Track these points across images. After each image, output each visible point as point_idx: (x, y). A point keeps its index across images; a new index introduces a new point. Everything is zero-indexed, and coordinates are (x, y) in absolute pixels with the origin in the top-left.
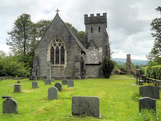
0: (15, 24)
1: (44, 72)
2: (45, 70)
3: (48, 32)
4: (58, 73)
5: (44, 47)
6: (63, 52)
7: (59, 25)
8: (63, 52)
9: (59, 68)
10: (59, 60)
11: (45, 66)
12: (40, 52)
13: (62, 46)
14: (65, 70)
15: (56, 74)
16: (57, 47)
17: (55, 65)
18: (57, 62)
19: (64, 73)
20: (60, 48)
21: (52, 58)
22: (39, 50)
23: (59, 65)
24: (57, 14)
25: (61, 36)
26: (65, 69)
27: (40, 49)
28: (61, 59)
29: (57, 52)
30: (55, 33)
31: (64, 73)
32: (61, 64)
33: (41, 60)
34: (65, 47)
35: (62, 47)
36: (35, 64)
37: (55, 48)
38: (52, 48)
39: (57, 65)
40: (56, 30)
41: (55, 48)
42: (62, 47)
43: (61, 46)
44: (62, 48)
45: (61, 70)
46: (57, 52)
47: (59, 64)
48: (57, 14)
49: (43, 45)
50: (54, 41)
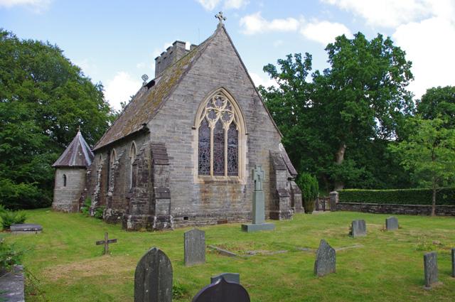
0: (37, 41)
1: (182, 198)
2: (184, 195)
3: (197, 72)
4: (225, 202)
5: (181, 117)
6: (234, 141)
7: (228, 60)
8: (234, 141)
9: (228, 188)
10: (224, 163)
11: (187, 181)
12: (168, 131)
13: (233, 122)
14: (244, 192)
15: (218, 205)
16: (220, 125)
17: (214, 178)
18: (219, 170)
19: (240, 202)
20: (227, 126)
21: (204, 156)
22: (165, 126)
23: (226, 178)
24: (221, 28)
25: (233, 91)
26: (242, 190)
27: (170, 122)
28: (229, 161)
29: (219, 138)
30: (217, 81)
31: (240, 202)
32: (228, 174)
33: (172, 158)
34: (241, 127)
35: (233, 125)
36: (162, 170)
37: (213, 124)
38: (205, 125)
39: (219, 178)
40: (220, 72)
41: (213, 124)
42: (233, 125)
43: (217, 119)
44: (230, 127)
45: (234, 192)
46: (219, 139)
47: (223, 174)
48: (221, 28)
49: (179, 110)
50: (211, 104)
